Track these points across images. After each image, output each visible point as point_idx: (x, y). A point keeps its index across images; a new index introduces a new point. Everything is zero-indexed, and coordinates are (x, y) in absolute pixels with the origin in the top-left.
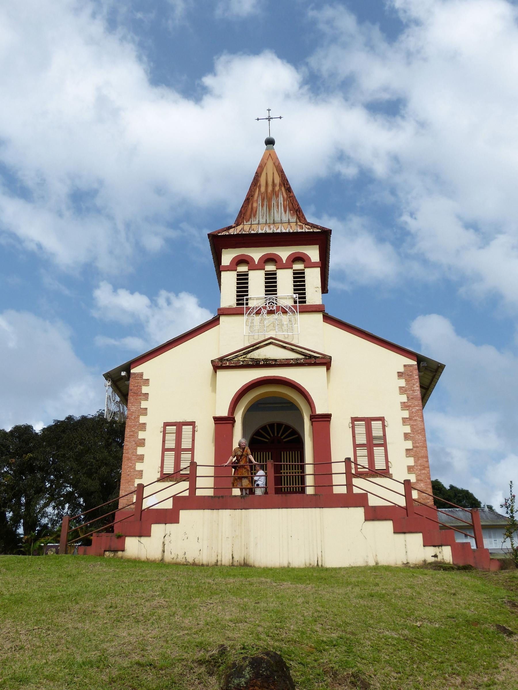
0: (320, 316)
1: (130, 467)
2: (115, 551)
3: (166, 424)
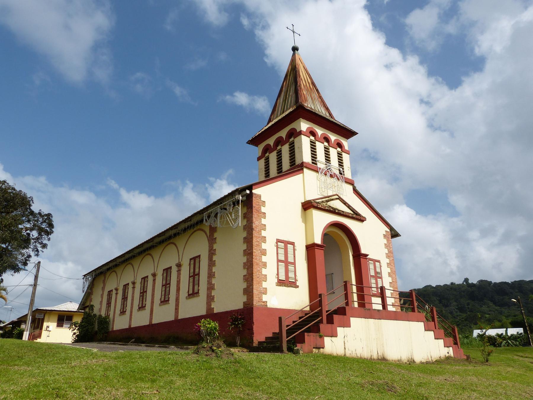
1: (259, 271)
2: (319, 348)
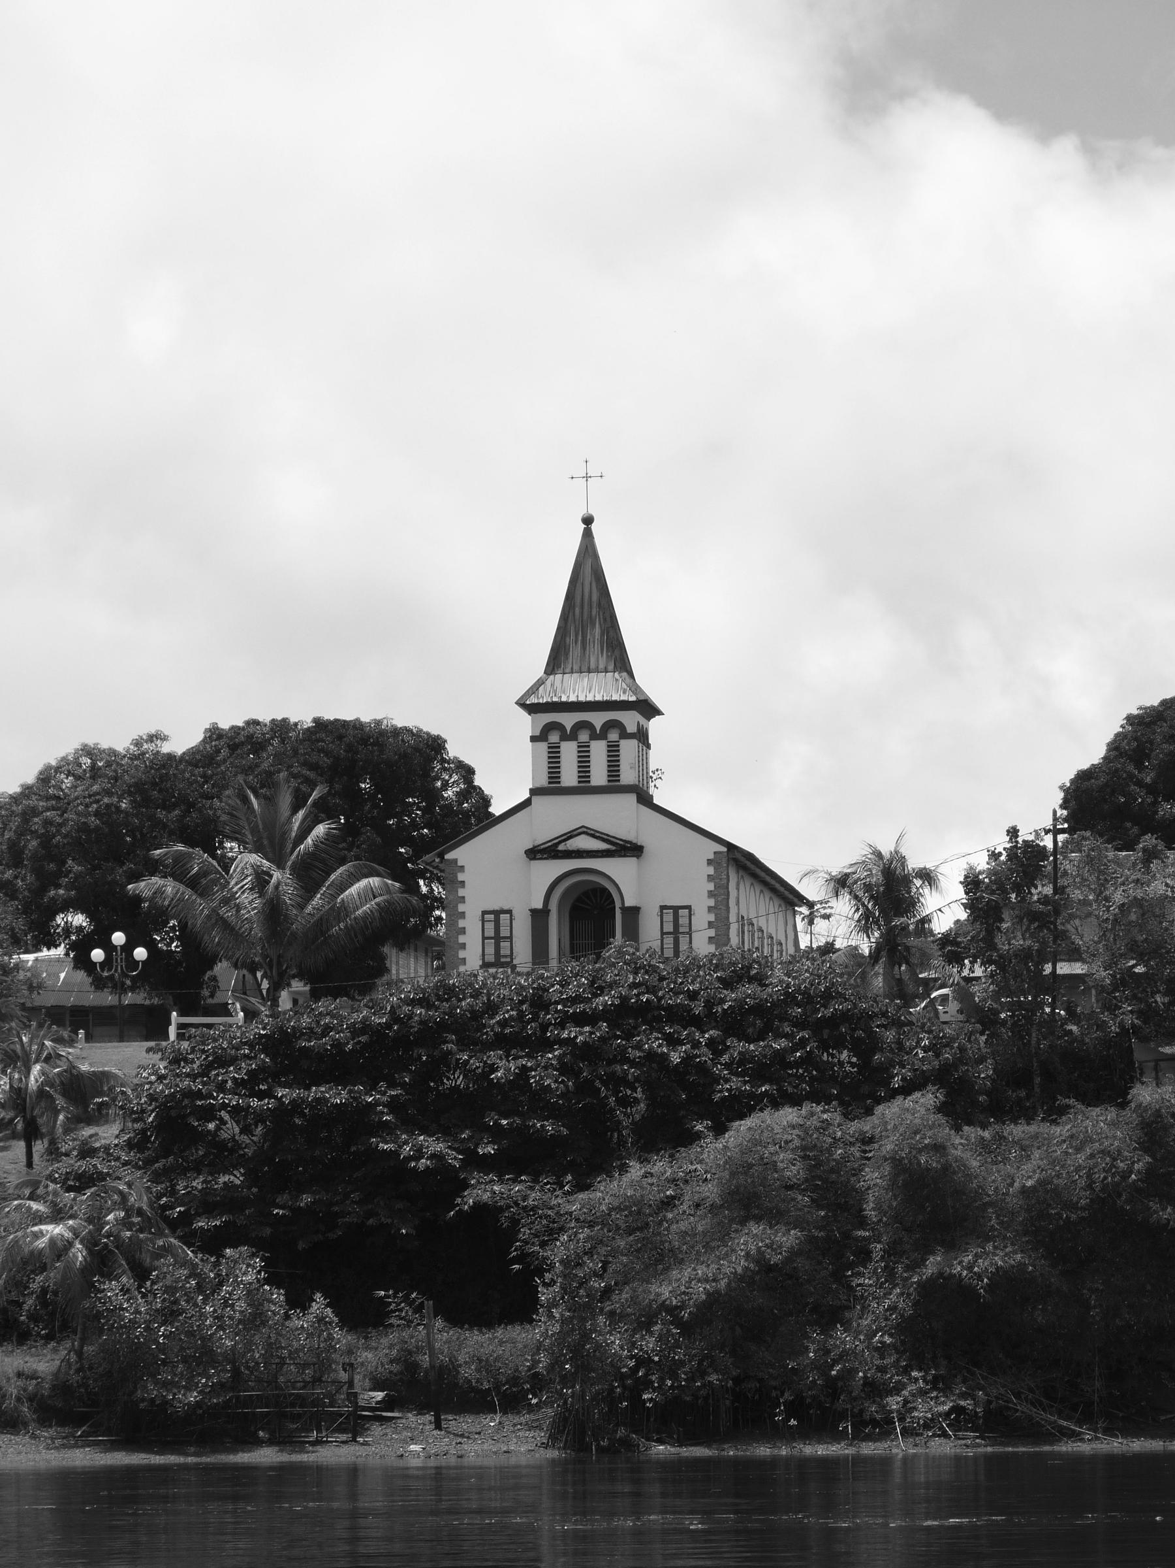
3: (484, 913)
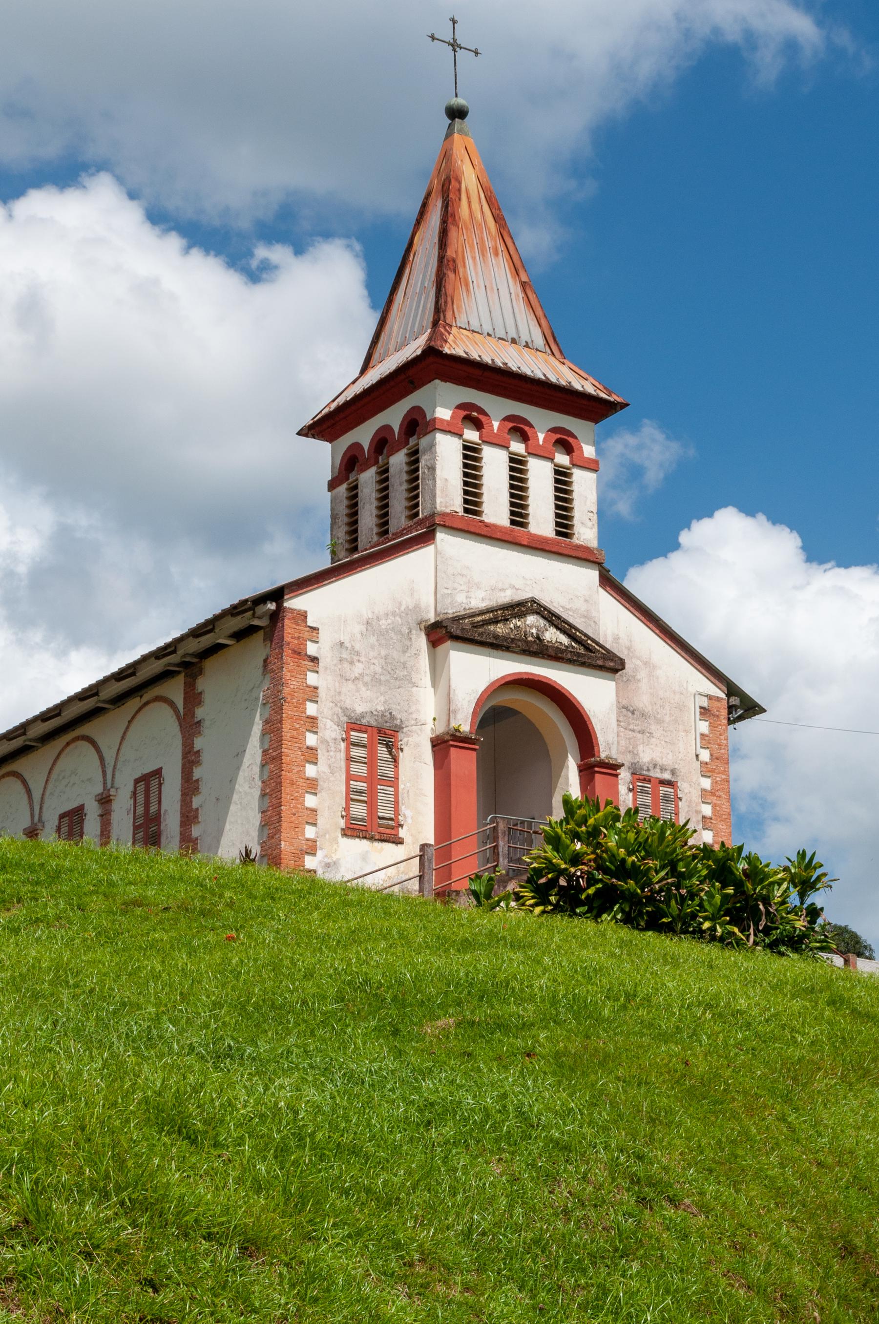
0: (593, 575)
1: (296, 799)
